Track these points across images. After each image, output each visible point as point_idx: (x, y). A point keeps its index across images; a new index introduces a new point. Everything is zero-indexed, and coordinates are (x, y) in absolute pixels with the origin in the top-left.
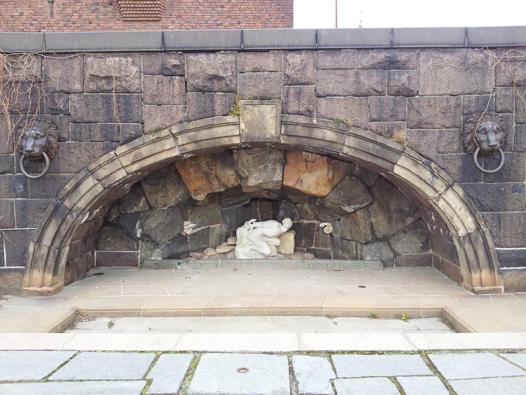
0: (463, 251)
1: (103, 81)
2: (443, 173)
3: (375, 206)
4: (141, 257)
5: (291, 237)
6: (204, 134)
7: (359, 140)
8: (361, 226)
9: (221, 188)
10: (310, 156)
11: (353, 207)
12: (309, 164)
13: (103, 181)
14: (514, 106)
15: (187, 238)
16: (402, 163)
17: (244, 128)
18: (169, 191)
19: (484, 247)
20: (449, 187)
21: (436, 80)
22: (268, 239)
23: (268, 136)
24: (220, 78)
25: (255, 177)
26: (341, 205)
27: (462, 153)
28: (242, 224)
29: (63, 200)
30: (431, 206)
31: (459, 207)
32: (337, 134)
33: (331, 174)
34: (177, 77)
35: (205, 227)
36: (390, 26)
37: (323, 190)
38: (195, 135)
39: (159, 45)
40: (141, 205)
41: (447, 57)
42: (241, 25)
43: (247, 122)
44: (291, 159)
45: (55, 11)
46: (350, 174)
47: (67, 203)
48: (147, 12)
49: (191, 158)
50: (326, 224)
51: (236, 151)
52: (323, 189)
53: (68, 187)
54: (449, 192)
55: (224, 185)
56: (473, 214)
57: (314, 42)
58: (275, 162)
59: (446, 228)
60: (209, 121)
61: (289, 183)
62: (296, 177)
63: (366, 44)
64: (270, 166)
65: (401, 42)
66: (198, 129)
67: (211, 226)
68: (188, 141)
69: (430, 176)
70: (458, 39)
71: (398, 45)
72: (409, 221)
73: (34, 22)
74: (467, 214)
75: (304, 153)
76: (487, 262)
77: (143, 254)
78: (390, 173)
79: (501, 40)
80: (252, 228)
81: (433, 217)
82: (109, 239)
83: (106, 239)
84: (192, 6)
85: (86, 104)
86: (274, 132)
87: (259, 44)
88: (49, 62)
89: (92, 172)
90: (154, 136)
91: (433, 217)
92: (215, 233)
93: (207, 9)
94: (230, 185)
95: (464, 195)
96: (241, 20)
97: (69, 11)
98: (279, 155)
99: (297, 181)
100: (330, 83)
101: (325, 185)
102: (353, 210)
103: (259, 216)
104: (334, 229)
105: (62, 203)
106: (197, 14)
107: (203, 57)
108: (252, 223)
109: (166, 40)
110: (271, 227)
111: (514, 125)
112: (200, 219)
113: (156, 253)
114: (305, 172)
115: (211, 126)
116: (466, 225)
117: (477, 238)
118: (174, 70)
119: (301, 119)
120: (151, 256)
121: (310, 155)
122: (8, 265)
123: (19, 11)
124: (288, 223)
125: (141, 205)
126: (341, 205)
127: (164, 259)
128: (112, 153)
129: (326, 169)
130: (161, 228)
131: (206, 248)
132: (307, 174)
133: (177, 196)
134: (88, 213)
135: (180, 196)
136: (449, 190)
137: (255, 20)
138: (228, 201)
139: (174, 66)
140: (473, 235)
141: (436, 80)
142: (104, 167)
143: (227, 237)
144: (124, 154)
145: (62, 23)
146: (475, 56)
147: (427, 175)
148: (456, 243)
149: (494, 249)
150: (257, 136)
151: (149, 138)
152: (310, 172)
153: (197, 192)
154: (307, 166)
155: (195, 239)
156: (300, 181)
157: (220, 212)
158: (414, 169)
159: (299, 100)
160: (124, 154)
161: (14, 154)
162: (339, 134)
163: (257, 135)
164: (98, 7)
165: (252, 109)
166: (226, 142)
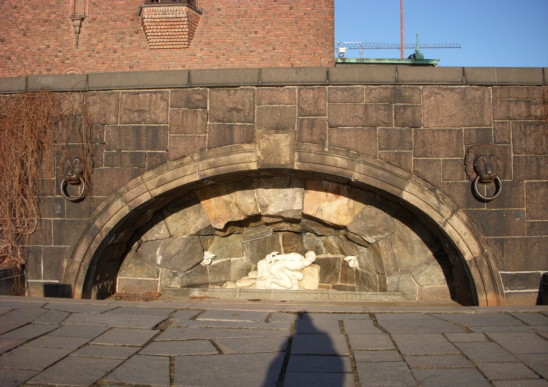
1: (135, 114)
2: (447, 199)
4: (161, 285)
5: (316, 269)
7: (369, 167)
9: (240, 216)
10: (330, 185)
13: (130, 203)
14: (511, 137)
15: (206, 270)
16: (409, 190)
17: (260, 155)
18: (189, 219)
19: (488, 270)
20: (454, 212)
21: (439, 112)
23: (282, 163)
24: (238, 111)
25: (275, 206)
27: (465, 181)
28: (263, 257)
29: (95, 220)
31: (464, 232)
32: (348, 162)
34: (200, 110)
35: (225, 260)
39: (186, 82)
40: (162, 232)
42: (276, 51)
43: (263, 149)
45: (80, 42)
47: (97, 223)
48: (175, 40)
49: (212, 185)
51: (256, 179)
53: (100, 208)
54: (455, 217)
55: (243, 213)
56: (477, 238)
57: (326, 79)
63: (373, 80)
65: (405, 79)
67: (232, 259)
69: (436, 202)
71: (403, 82)
73: (60, 54)
74: (472, 238)
75: (324, 182)
76: (492, 286)
77: (163, 282)
80: (273, 261)
82: (130, 266)
83: (127, 265)
85: (119, 134)
86: (288, 159)
87: (275, 81)
89: (121, 195)
90: (177, 162)
92: (236, 266)
94: (249, 213)
95: (468, 220)
97: (94, 41)
99: (318, 211)
101: (346, 215)
103: (282, 249)
105: (93, 223)
107: (222, 94)
108: (273, 256)
109: (192, 78)
110: (294, 260)
111: (512, 155)
112: (220, 250)
113: (175, 281)
114: (324, 201)
116: (471, 249)
117: (481, 262)
118: (198, 103)
119: (314, 147)
120: (171, 284)
121: (330, 184)
123: (47, 44)
124: (311, 256)
125: (162, 232)
127: (182, 287)
128: (139, 177)
130: (181, 255)
131: (225, 282)
133: (197, 224)
134: (115, 235)
135: (200, 225)
136: (454, 215)
138: (249, 233)
139: (198, 100)
140: (478, 259)
142: (131, 191)
143: (248, 270)
144: (150, 179)
145: (86, 54)
146: (475, 93)
147: (433, 200)
150: (272, 162)
151: (173, 164)
155: (214, 271)
157: (241, 244)
158: (421, 196)
159: (312, 129)
160: (150, 179)
162: (350, 162)
163: (272, 162)
164: (123, 36)
165: (268, 138)
166: (243, 167)
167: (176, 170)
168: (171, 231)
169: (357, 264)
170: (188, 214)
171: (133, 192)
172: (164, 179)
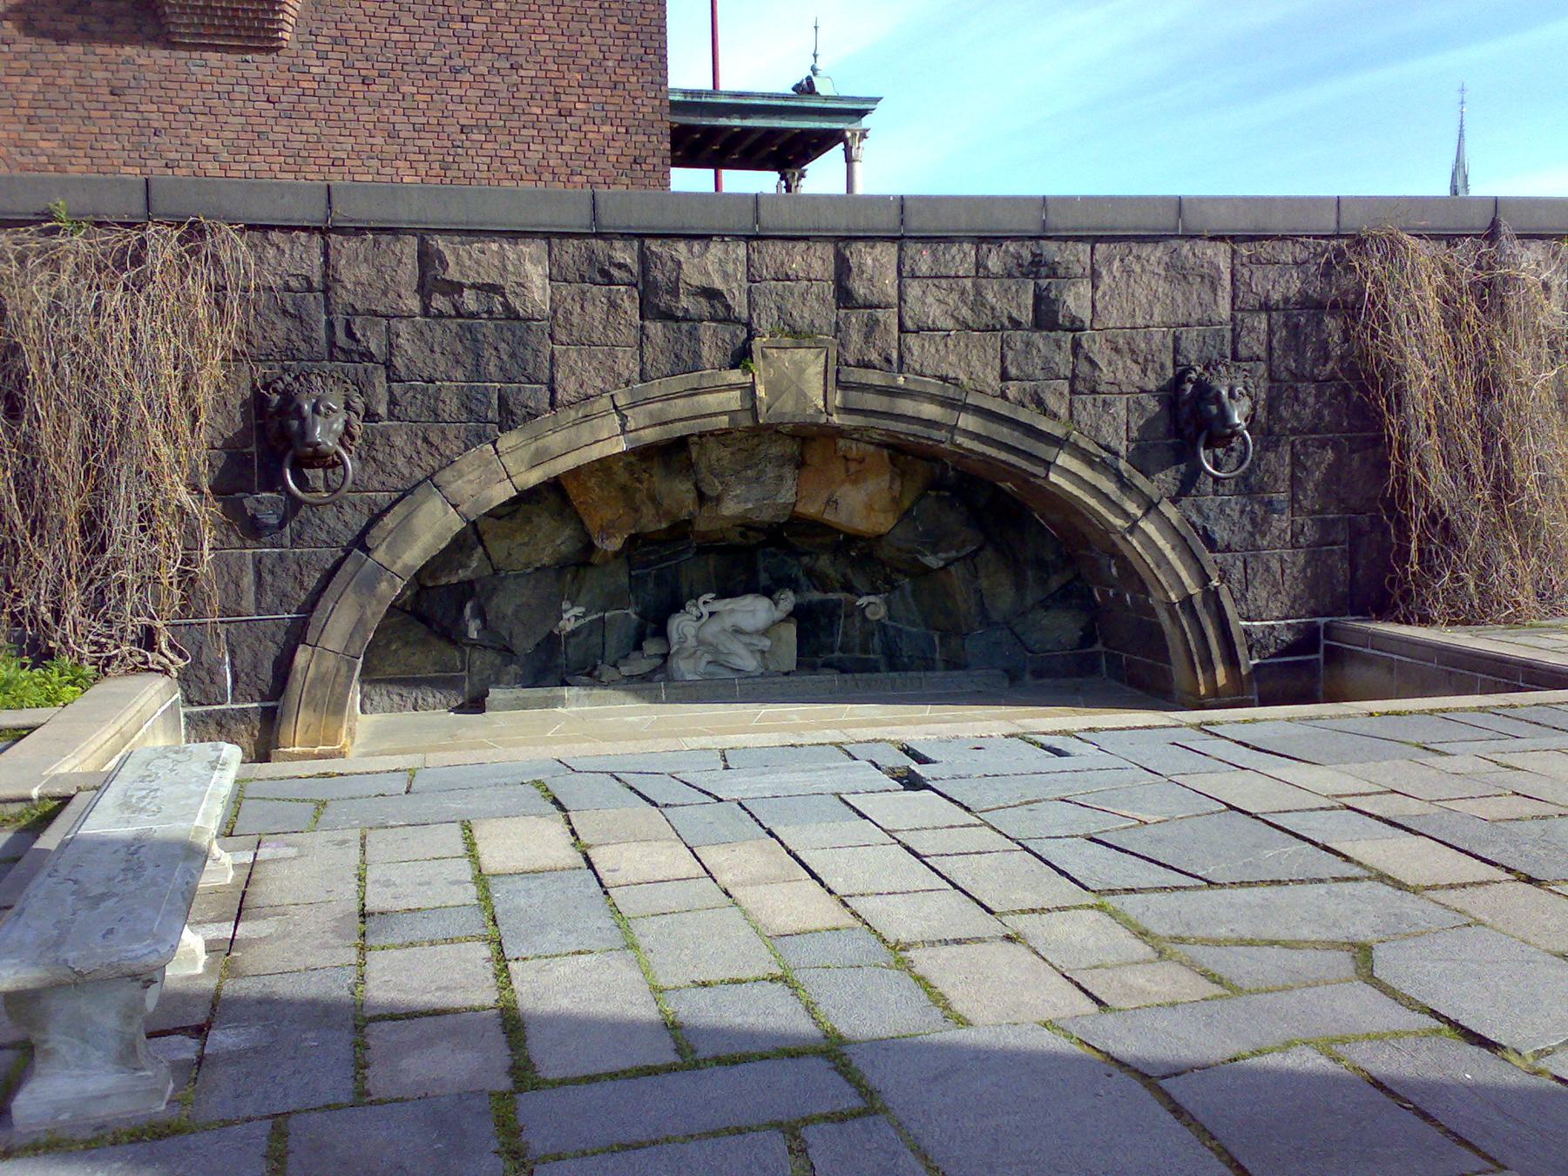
0: (1178, 632)
3: (988, 553)
5: (790, 632)
6: (680, 407)
8: (959, 598)
11: (943, 555)
12: (853, 467)
18: (540, 530)
22: (746, 639)
26: (919, 552)
30: (1114, 544)
33: (897, 486)
36: (1041, 193)
37: (881, 522)
38: (661, 410)
40: (474, 564)
41: (1146, 250)
44: (815, 456)
46: (935, 484)
50: (872, 599)
52: (881, 518)
55: (668, 513)
57: (898, 223)
58: (782, 461)
59: (1143, 588)
60: (692, 379)
61: (811, 509)
62: (824, 496)
64: (771, 472)
65: (1060, 225)
66: (667, 398)
68: (648, 422)
70: (1165, 221)
72: (1055, 582)
75: (841, 443)
78: (1039, 482)
79: (1244, 224)
81: (1114, 571)
84: (379, 13)
88: (345, 247)
91: (1114, 571)
93: (423, 23)
95: (1180, 521)
96: (521, 60)
98: (791, 448)
100: (929, 304)
102: (942, 564)
104: (889, 610)
106: (395, 37)
110: (754, 611)
114: (842, 483)
115: (695, 392)
122: (235, 701)
126: (919, 552)
129: (887, 477)
132: (848, 486)
137: (561, 60)
141: (1130, 307)
144: (514, 449)
148: (1164, 617)
149: (1238, 625)
152: (855, 482)
153: (607, 530)
154: (847, 470)
156: (832, 502)
161: (253, 449)
167: (573, 430)
168: (495, 560)
169: (883, 611)
170: (536, 520)
171: (471, 482)
172: (547, 448)
